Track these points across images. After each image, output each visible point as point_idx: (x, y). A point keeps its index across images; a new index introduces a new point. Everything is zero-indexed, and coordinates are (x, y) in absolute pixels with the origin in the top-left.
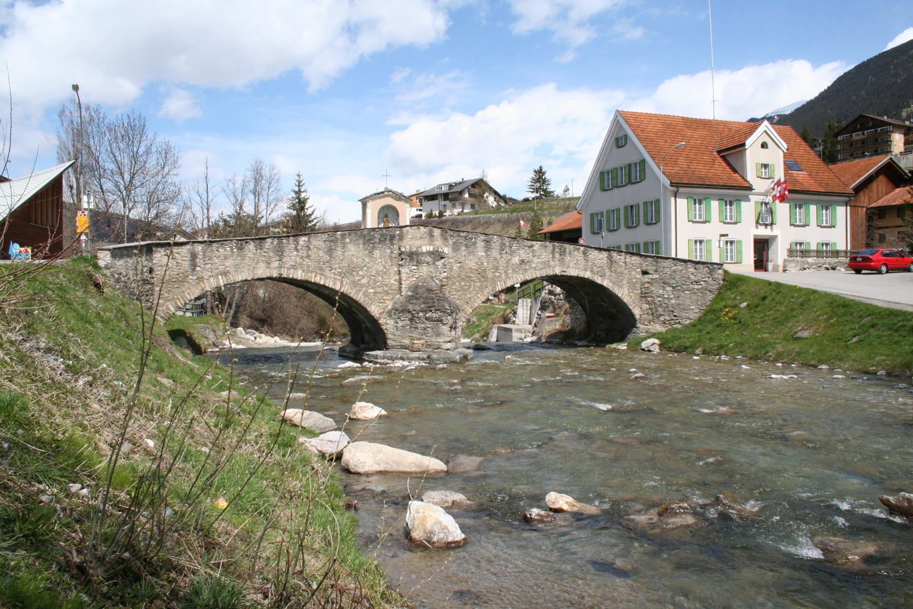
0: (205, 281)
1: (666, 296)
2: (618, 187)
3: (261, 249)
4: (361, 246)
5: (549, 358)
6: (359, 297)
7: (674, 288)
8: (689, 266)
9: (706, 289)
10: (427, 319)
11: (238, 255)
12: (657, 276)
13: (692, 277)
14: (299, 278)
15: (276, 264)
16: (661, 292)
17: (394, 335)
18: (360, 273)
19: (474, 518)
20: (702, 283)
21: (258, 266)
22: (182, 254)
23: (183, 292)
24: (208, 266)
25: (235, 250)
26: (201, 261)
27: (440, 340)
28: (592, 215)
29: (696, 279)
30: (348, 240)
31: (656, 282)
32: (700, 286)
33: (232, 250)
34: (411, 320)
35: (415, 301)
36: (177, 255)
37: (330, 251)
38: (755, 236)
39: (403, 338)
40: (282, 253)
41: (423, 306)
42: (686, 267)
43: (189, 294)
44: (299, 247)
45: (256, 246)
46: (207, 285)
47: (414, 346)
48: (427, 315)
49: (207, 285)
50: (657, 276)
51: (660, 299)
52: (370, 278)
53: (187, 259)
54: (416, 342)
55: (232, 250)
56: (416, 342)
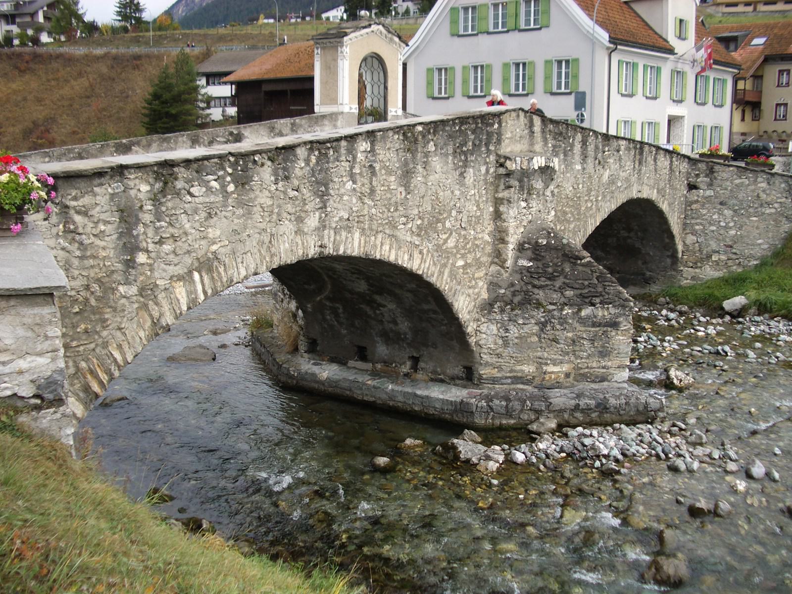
0: (161, 296)
1: (722, 224)
2: (517, 29)
3: (287, 178)
4: (450, 158)
5: (185, 253)
6: (443, 282)
7: (735, 211)
8: (759, 179)
9: (783, 215)
10: (583, 321)
11: (240, 204)
12: (709, 193)
13: (763, 196)
14: (355, 254)
15: (312, 221)
16: (715, 217)
17: (499, 356)
18: (448, 224)
19: (72, 469)
20: (776, 205)
21: (282, 229)
22: (94, 212)
23: (105, 345)
24: (167, 248)
25: (231, 188)
26: (150, 232)
27: (610, 364)
28: (430, 71)
29: (769, 199)
30: (431, 147)
31: (709, 202)
32: (773, 211)
33: (224, 187)
34: (543, 325)
35: (543, 282)
36: (78, 218)
37: (407, 175)
38: (669, 116)
39: (519, 362)
40: (327, 189)
41: (569, 293)
42: (755, 181)
43: (120, 347)
44: (357, 170)
45: (275, 173)
46: (166, 307)
47: (547, 377)
48: (583, 313)
49: (166, 307)
50: (709, 193)
51: (714, 228)
52: (459, 234)
53: (109, 229)
54: (551, 368)
55: (224, 187)
56: (551, 368)
